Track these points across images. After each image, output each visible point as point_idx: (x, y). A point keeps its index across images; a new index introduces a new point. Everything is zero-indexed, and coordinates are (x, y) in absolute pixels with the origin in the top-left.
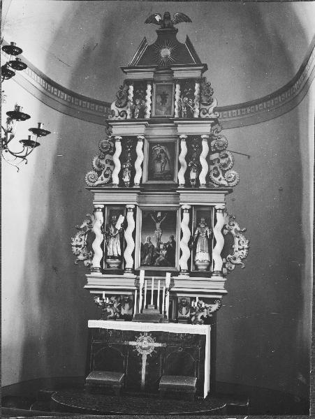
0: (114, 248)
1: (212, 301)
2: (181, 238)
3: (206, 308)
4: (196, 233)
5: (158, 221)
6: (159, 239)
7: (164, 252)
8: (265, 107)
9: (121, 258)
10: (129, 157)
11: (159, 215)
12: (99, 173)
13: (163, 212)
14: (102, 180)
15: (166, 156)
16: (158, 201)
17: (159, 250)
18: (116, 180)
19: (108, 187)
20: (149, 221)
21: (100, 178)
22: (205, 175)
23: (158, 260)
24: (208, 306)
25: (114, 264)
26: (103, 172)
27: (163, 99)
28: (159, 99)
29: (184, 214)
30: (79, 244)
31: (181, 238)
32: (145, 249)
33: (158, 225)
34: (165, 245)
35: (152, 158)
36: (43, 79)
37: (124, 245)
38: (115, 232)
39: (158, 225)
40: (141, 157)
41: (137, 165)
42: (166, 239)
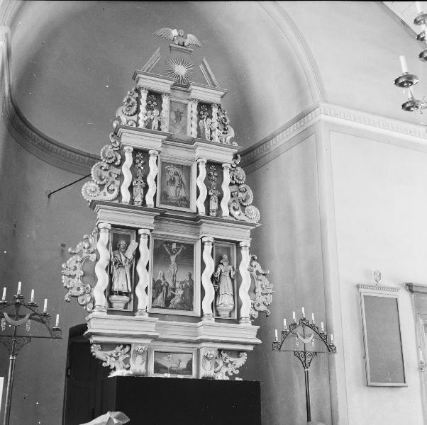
0: (121, 283)
1: (237, 353)
2: (147, 288)
3: (231, 363)
4: (219, 270)
5: (172, 254)
6: (173, 274)
7: (180, 292)
8: (299, 126)
9: (131, 294)
10: (140, 172)
11: (174, 246)
12: (102, 186)
13: (178, 244)
14: (105, 195)
15: (181, 180)
16: (181, 233)
17: (174, 290)
18: (126, 197)
19: (116, 203)
20: (161, 251)
21: (102, 192)
22: (223, 199)
23: (175, 300)
24: (232, 359)
25: (119, 302)
26: (106, 187)
27: (177, 117)
28: (174, 117)
29: (205, 247)
30: (72, 273)
31: (147, 288)
32: (157, 287)
33: (173, 258)
34: (182, 283)
35: (163, 179)
36: (13, 105)
37: (135, 280)
38: (126, 261)
39: (173, 258)
40: (154, 170)
41: (150, 180)
42: (182, 276)
